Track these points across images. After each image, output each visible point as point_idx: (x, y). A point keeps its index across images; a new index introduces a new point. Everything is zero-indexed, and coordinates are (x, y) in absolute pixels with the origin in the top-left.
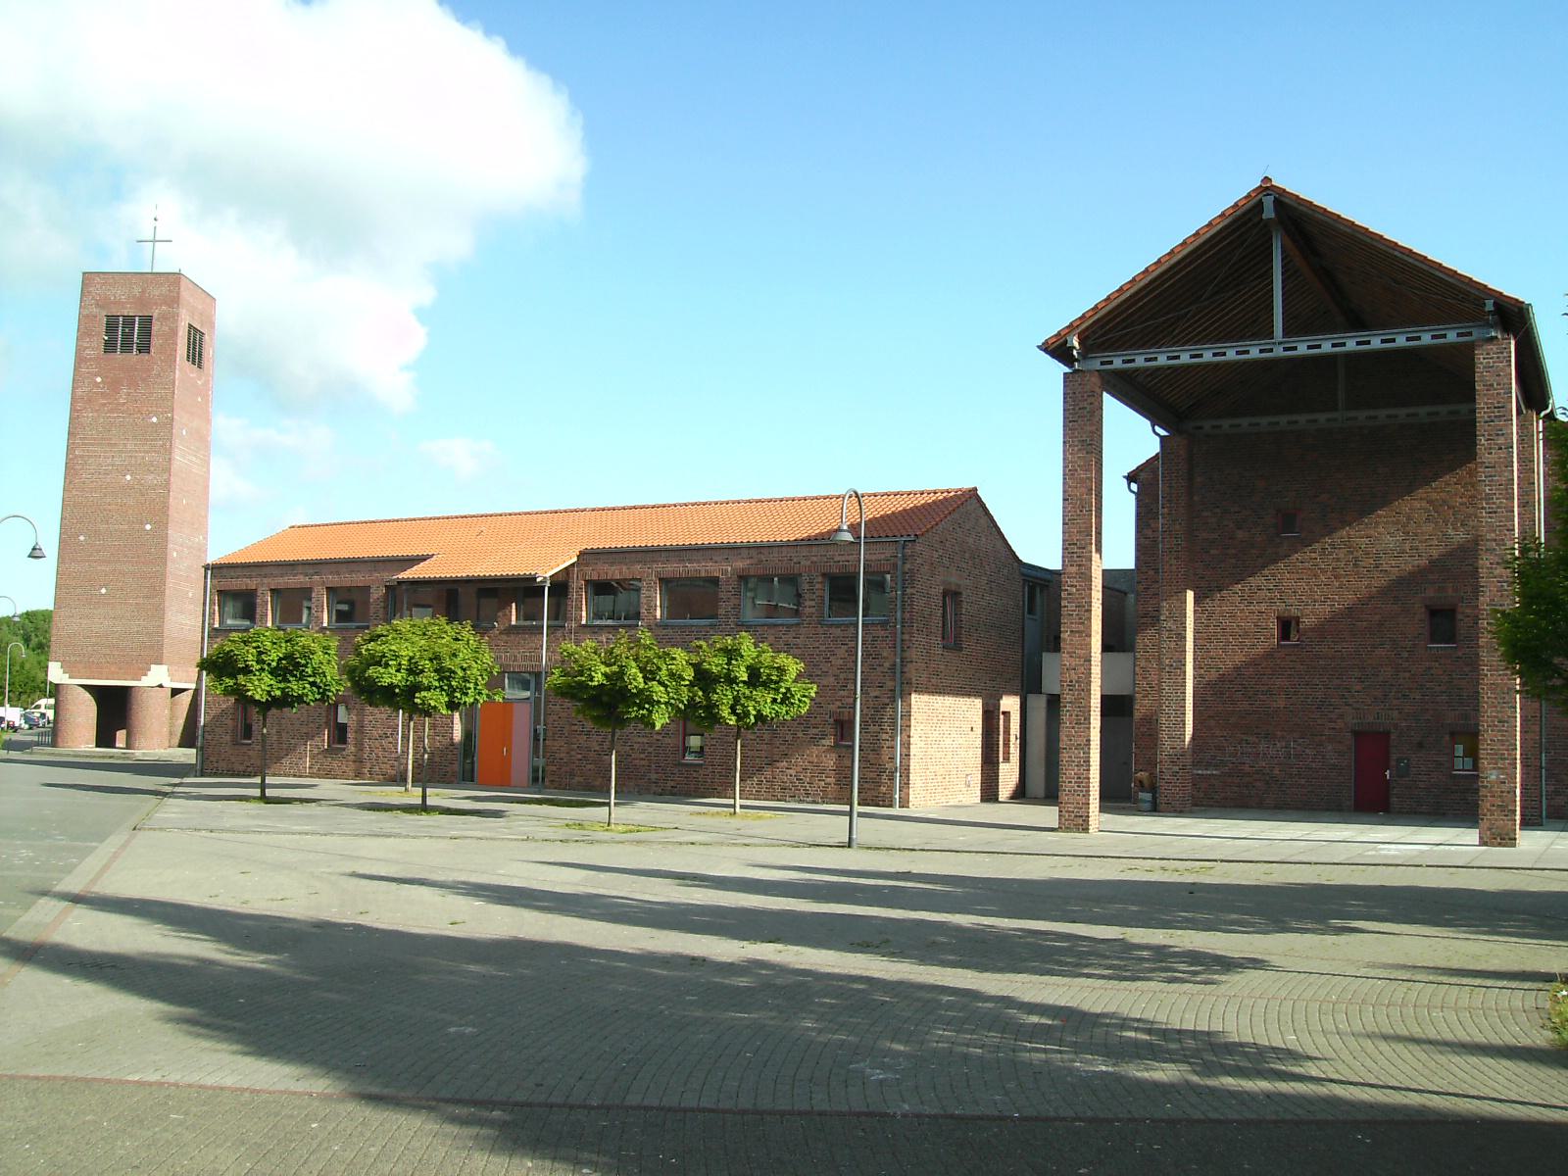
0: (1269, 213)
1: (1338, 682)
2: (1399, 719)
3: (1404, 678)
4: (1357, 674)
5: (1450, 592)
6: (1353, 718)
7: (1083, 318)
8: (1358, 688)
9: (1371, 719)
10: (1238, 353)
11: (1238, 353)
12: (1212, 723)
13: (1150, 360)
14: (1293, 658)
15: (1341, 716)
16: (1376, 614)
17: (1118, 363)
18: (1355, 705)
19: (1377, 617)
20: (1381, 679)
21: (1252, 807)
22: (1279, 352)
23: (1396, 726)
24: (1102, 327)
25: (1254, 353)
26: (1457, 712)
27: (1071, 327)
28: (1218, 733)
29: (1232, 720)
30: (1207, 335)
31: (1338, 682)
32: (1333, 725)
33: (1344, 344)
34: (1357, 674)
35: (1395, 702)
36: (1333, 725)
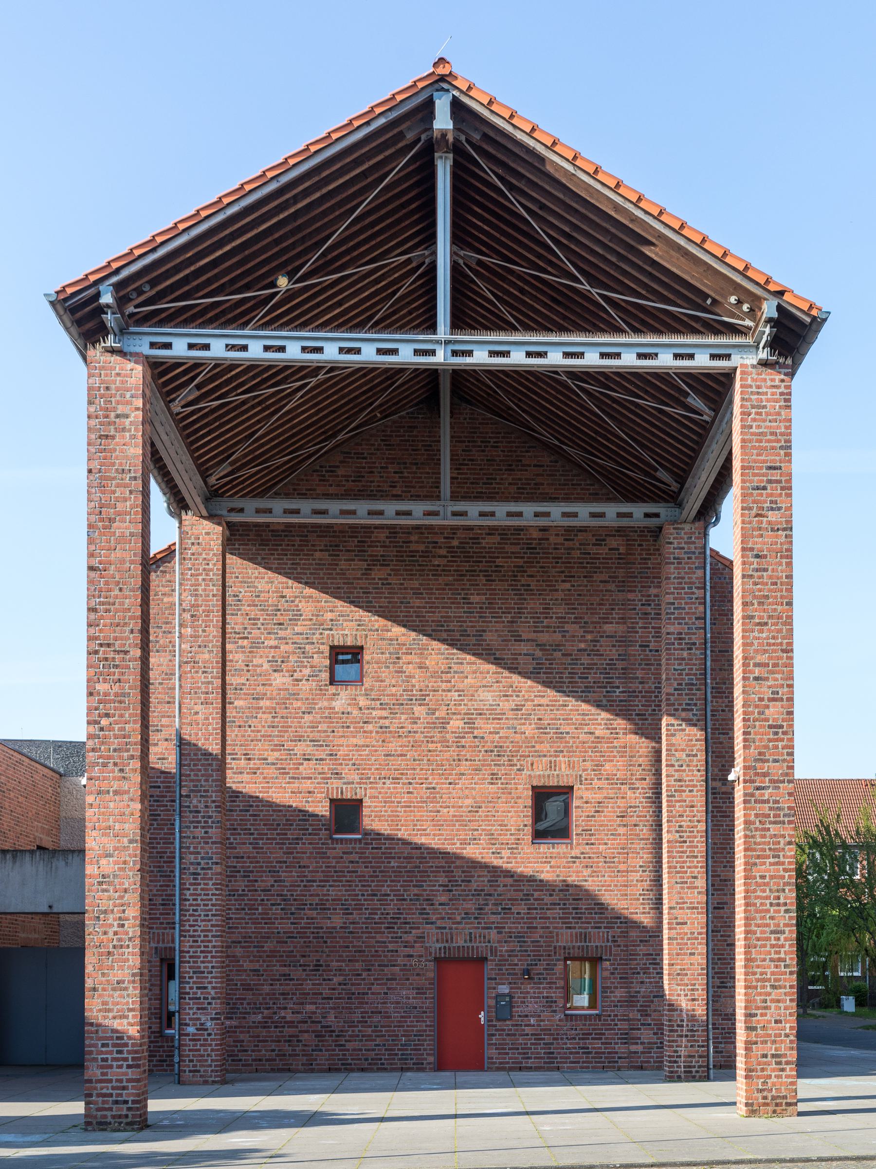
0: (443, 121)
1: (416, 891)
2: (499, 942)
3: (505, 886)
4: (443, 880)
5: (564, 770)
6: (437, 941)
7: (130, 258)
8: (443, 899)
9: (461, 943)
10: (417, 352)
11: (304, 349)
12: (238, 951)
13: (349, 351)
14: (355, 857)
15: (421, 938)
16: (467, 797)
17: (180, 348)
18: (439, 923)
19: (468, 802)
20: (474, 886)
21: (297, 1071)
22: (440, 357)
23: (493, 951)
24: (153, 283)
25: (406, 355)
26: (574, 931)
27: (109, 272)
28: (247, 965)
29: (268, 946)
30: (396, 321)
31: (416, 891)
32: (410, 951)
33: (358, 351)
34: (443, 880)
35: (493, 918)
36: (410, 951)
